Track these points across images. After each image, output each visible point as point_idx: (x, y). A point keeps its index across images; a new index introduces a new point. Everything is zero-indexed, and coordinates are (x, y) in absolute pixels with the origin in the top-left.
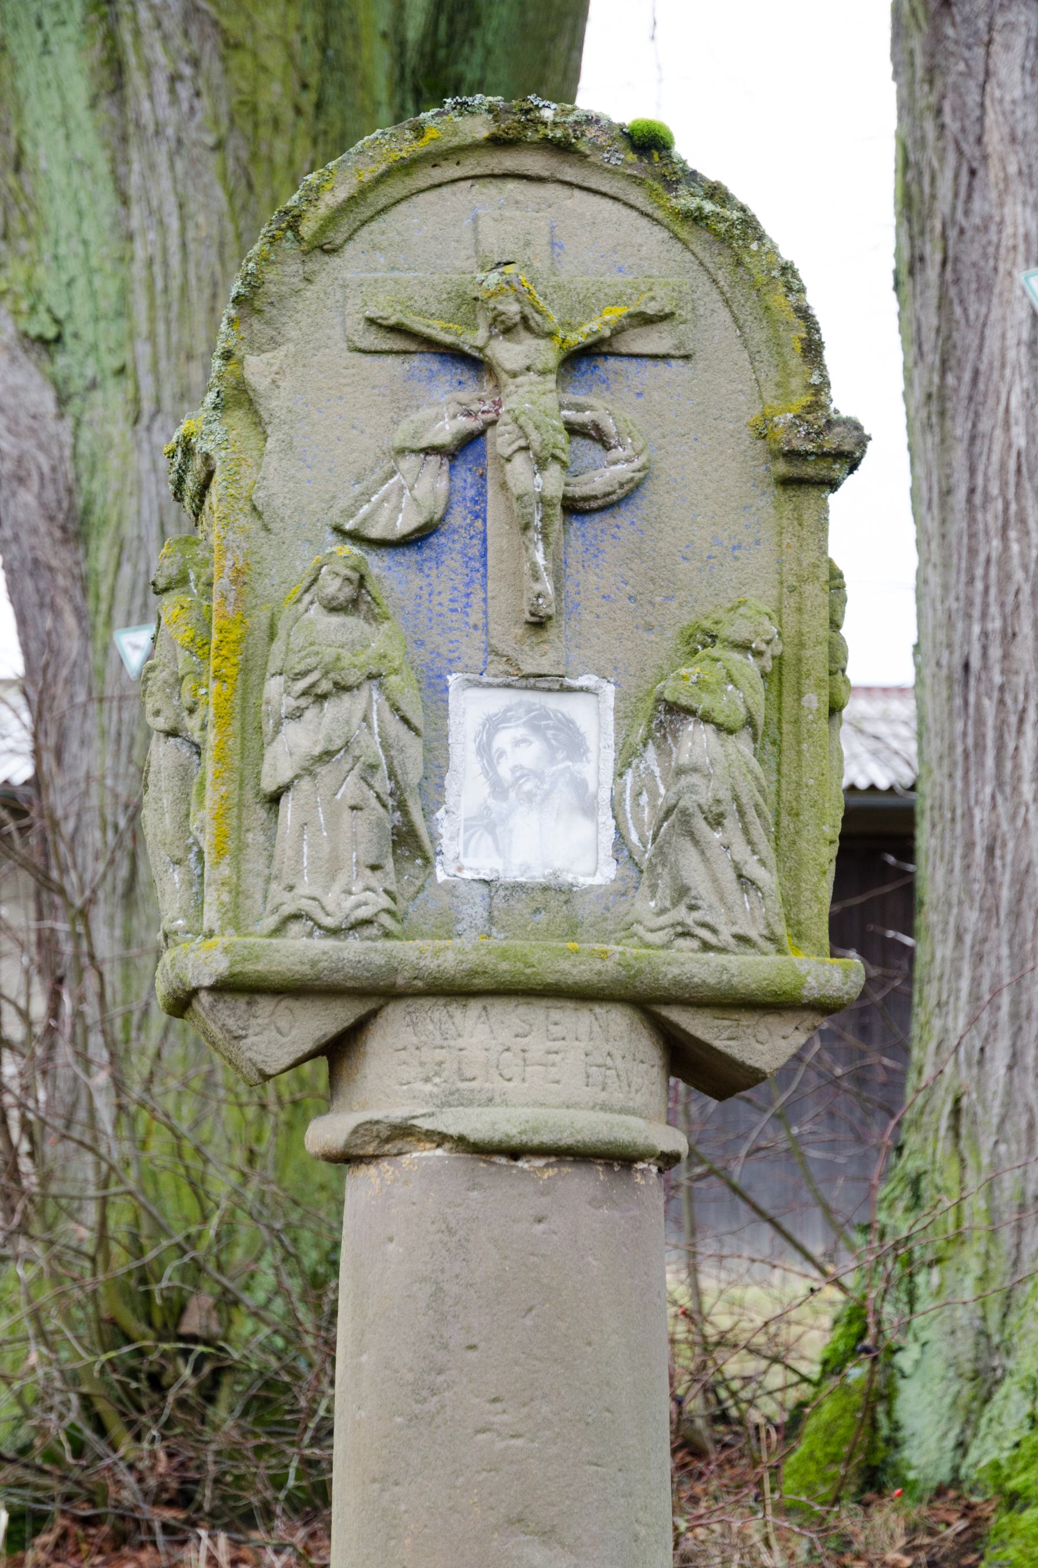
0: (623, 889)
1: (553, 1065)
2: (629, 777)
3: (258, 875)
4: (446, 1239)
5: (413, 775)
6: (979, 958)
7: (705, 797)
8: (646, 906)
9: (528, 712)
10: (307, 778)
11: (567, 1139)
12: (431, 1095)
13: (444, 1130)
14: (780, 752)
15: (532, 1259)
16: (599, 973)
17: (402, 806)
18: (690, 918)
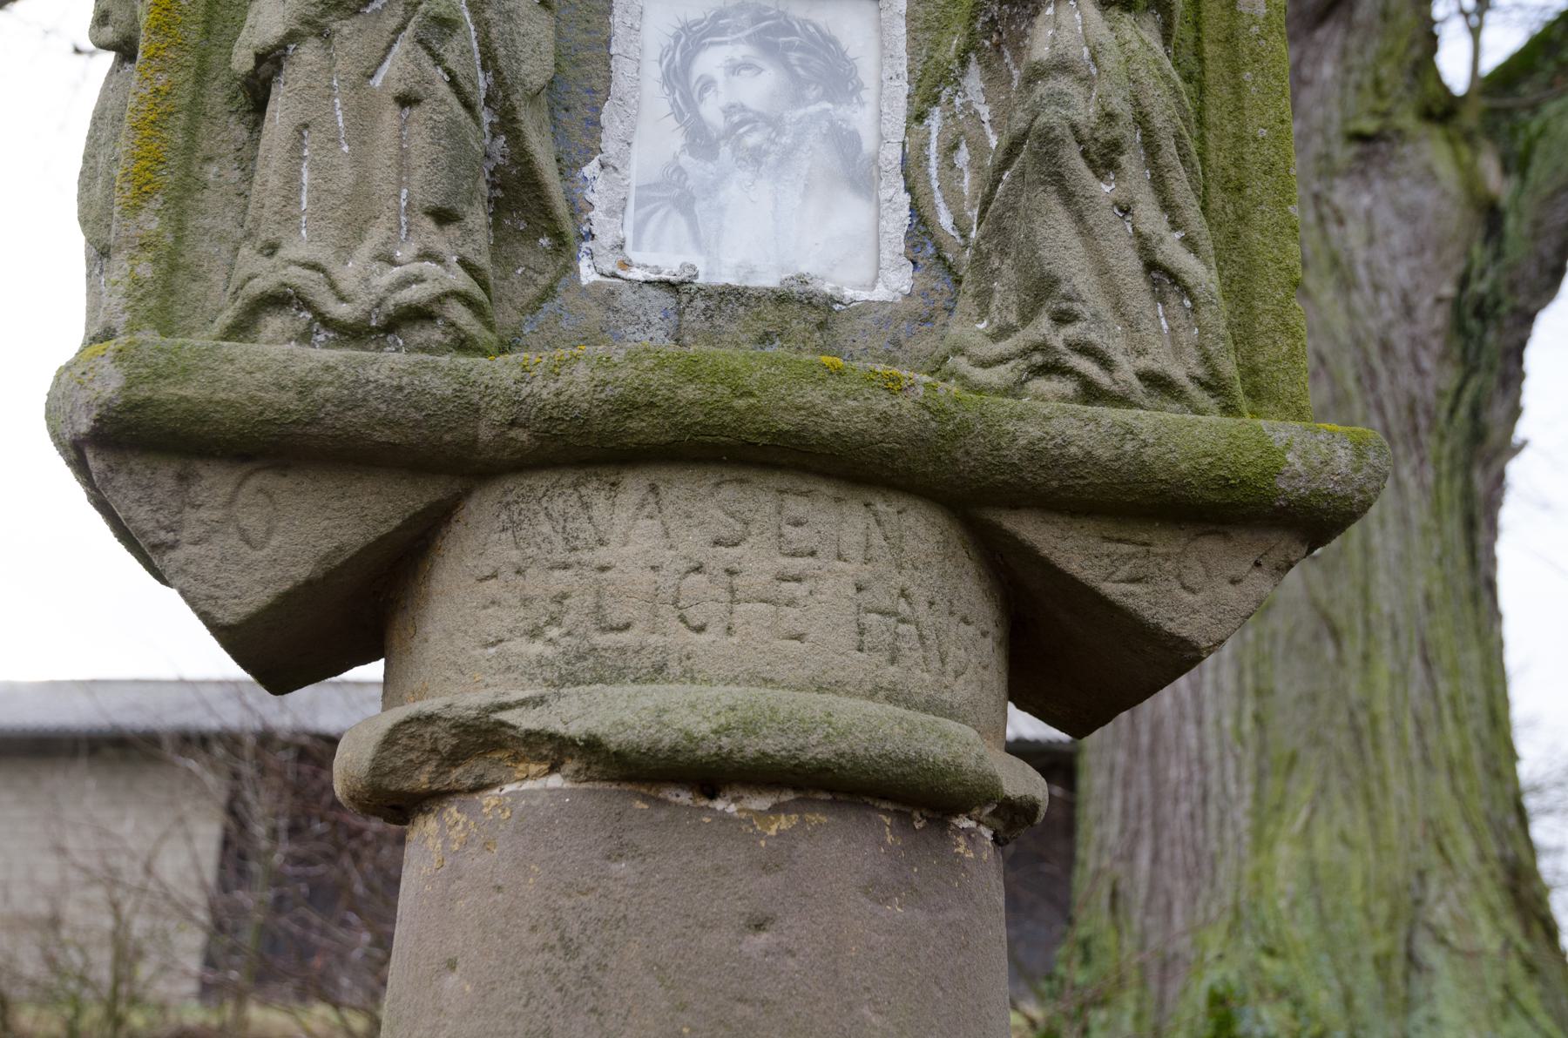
0: (925, 311)
1: (791, 603)
2: (935, 121)
3: (222, 238)
4: (558, 964)
5: (534, 69)
6: (1126, 785)
7: (1085, 112)
8: (971, 330)
9: (757, 19)
10: (312, 42)
11: (817, 749)
12: (541, 662)
13: (560, 729)
14: (1202, 91)
15: (741, 1010)
16: (885, 418)
17: (508, 125)
18: (1058, 339)
